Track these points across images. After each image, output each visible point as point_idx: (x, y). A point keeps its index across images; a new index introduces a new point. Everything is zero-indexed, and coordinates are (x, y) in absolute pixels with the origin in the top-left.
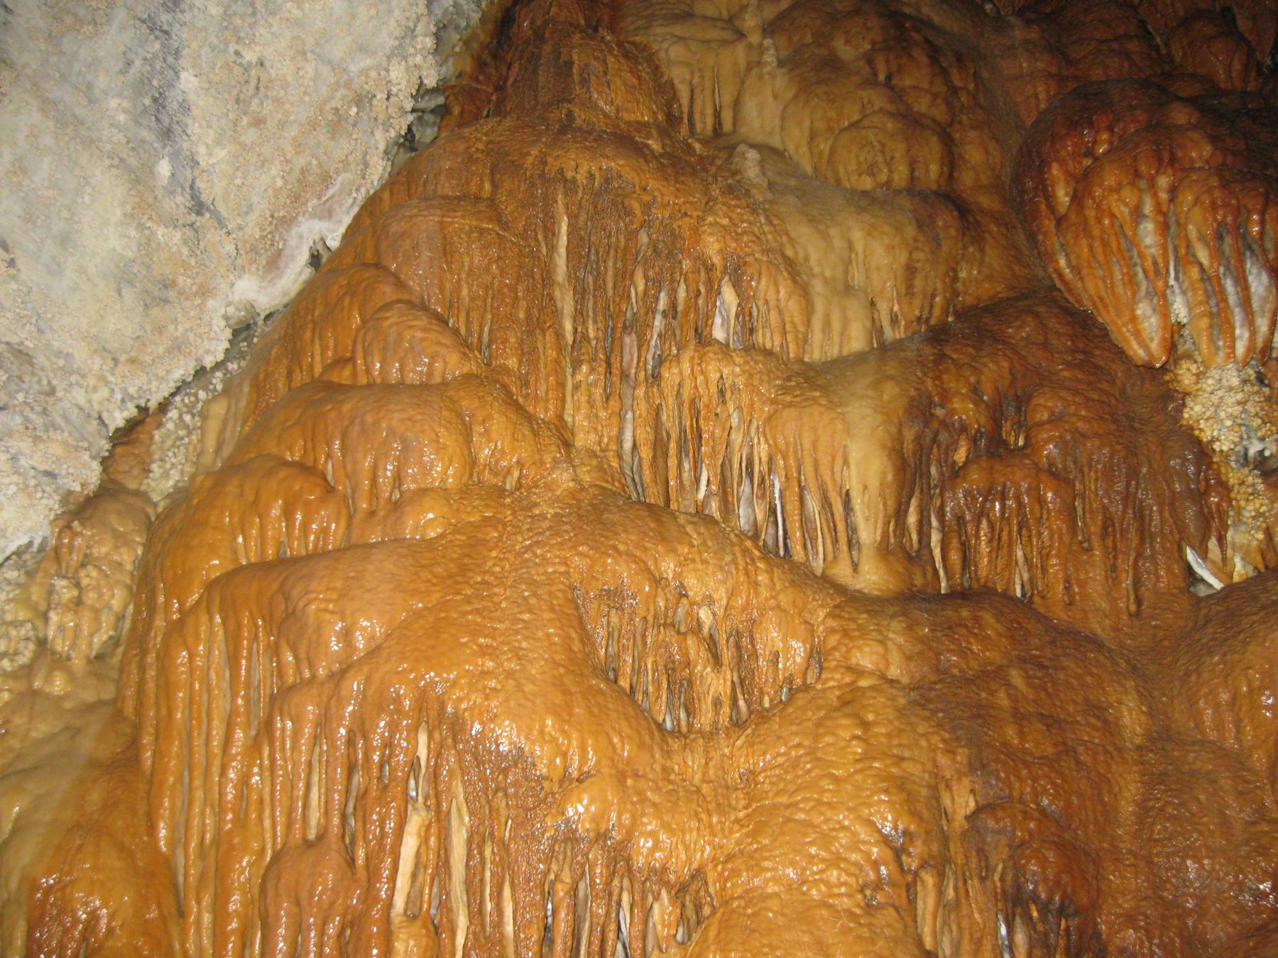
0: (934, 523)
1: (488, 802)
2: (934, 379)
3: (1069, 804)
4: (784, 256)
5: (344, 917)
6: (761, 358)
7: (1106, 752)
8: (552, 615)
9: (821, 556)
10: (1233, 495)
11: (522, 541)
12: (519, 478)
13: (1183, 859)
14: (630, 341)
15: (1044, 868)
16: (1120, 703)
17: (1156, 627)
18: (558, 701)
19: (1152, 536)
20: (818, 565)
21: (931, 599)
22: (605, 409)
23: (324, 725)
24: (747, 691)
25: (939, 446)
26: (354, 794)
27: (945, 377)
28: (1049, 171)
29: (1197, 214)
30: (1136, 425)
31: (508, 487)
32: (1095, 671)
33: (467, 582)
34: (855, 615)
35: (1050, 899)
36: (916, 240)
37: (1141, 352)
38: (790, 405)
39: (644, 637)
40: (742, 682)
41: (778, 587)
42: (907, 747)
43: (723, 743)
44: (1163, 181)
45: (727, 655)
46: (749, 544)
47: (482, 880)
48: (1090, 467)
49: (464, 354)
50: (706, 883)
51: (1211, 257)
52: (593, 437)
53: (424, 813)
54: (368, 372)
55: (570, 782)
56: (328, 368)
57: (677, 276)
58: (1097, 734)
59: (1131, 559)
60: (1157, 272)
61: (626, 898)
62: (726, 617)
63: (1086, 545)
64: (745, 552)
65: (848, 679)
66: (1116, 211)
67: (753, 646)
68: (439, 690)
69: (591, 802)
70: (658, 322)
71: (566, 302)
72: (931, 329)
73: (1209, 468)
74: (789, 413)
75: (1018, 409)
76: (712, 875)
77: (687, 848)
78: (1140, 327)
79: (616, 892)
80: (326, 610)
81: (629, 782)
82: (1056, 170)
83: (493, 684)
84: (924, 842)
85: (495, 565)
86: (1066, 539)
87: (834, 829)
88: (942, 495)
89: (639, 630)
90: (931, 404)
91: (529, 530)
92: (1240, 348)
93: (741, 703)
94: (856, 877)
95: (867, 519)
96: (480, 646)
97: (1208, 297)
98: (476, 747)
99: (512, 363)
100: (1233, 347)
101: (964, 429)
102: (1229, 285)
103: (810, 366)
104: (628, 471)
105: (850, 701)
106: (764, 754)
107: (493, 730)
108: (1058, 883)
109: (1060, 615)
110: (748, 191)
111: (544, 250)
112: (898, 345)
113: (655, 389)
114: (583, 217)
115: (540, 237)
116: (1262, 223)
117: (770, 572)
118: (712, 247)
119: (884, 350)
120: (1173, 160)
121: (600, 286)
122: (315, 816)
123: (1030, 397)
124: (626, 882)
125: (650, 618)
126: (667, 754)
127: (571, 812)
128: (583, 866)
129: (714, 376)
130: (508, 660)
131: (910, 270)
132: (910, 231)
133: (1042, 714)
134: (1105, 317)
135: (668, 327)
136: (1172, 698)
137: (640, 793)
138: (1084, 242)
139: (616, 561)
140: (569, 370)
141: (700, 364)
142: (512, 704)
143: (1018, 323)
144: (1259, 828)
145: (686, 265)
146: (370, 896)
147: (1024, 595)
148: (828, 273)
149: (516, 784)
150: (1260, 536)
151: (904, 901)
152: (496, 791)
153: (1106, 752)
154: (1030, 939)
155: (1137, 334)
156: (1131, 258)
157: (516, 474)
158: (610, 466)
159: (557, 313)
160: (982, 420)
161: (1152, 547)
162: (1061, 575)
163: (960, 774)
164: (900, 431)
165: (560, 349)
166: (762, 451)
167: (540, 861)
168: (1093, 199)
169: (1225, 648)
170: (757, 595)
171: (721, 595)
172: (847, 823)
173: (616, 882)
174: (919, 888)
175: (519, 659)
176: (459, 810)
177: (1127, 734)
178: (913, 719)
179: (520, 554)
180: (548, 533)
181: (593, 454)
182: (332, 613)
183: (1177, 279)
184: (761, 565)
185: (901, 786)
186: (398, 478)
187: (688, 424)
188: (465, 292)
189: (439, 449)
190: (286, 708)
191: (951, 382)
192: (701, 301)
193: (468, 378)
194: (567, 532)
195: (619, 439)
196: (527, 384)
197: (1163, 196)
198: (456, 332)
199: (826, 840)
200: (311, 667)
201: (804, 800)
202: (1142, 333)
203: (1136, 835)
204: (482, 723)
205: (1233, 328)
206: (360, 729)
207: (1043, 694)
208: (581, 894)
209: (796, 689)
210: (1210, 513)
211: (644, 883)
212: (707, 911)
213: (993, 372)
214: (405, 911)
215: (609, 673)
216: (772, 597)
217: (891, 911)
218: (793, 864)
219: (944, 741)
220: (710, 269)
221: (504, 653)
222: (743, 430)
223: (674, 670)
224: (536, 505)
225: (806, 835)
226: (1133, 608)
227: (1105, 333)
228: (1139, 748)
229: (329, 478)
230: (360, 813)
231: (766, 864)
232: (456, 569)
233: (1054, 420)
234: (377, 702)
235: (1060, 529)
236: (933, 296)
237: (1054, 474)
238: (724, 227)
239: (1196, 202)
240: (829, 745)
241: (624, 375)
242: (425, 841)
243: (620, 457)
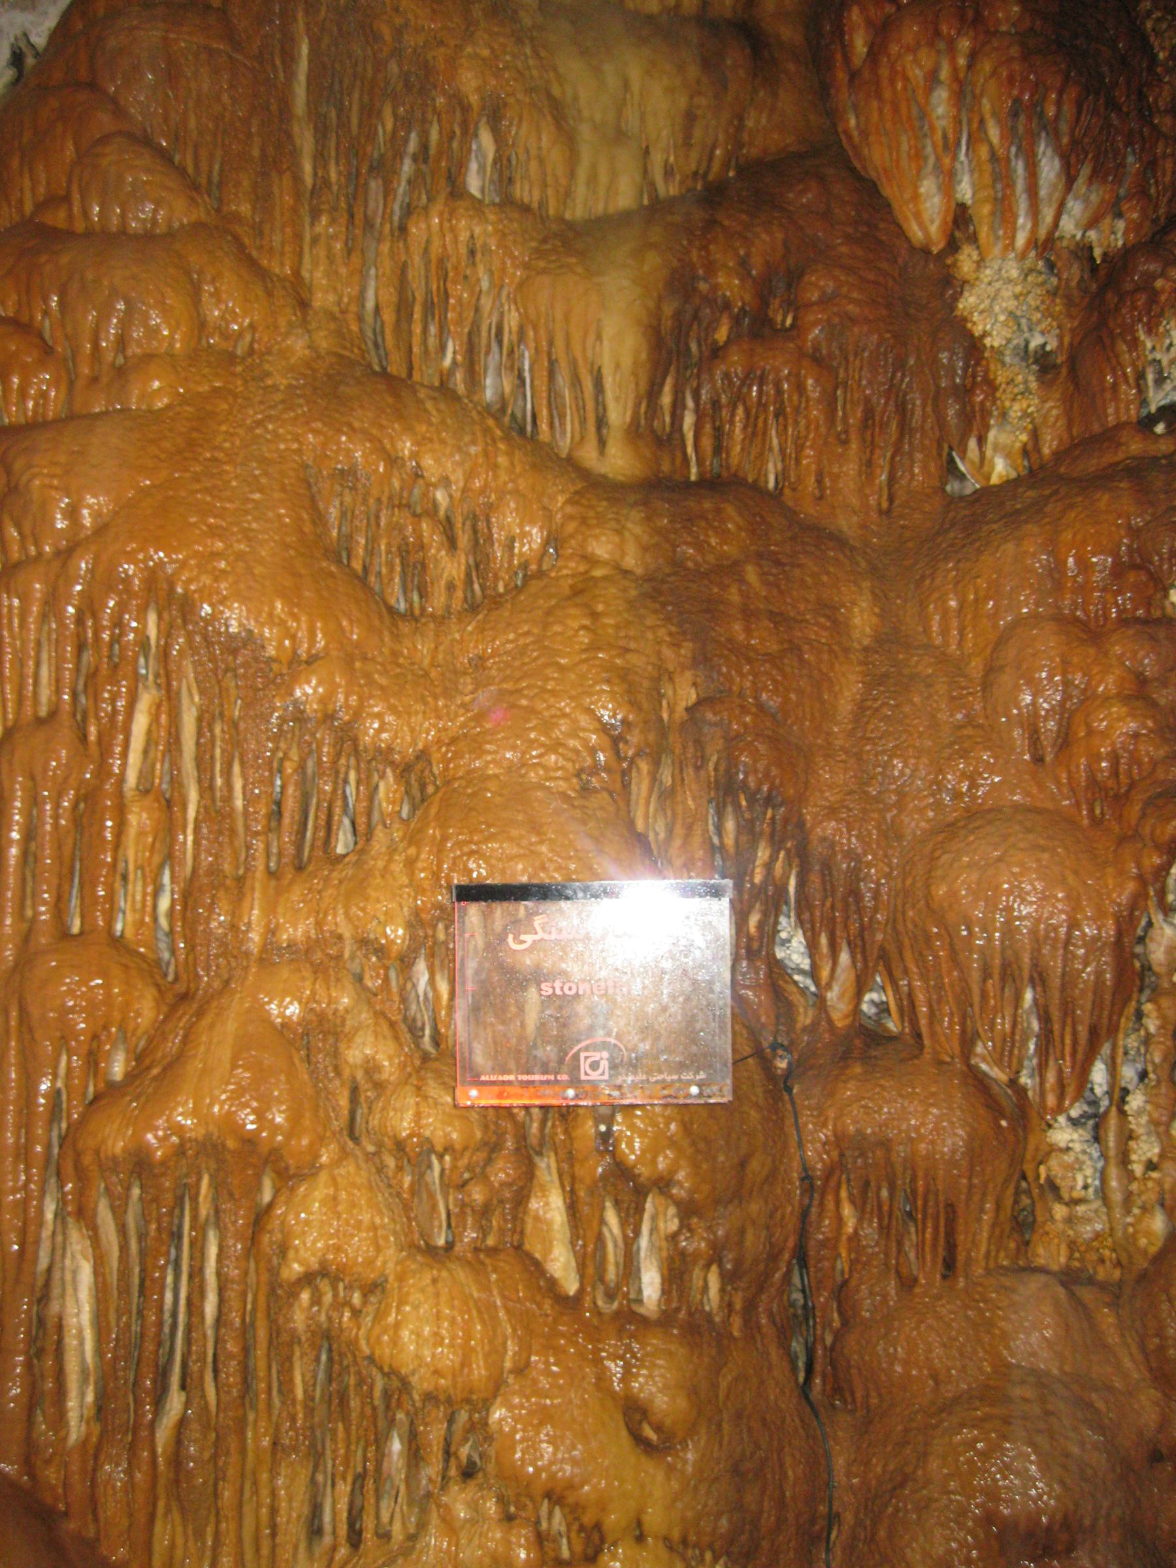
0: (690, 403)
1: (219, 682)
2: (700, 249)
3: (786, 700)
4: (550, 96)
5: (78, 790)
6: (516, 216)
7: (831, 651)
8: (282, 495)
9: (569, 435)
10: (998, 395)
11: (253, 414)
12: (252, 343)
13: (891, 757)
14: (375, 185)
15: (755, 761)
16: (854, 603)
17: (903, 527)
18: (286, 583)
19: (912, 432)
20: (564, 445)
21: (671, 490)
22: (347, 265)
23: (53, 603)
24: (482, 576)
25: (699, 325)
26: (84, 671)
27: (712, 247)
28: (849, 11)
29: (992, 85)
30: (912, 311)
31: (239, 352)
32: (832, 569)
33: (195, 459)
34: (594, 502)
35: (759, 790)
36: (698, 82)
37: (920, 234)
38: (544, 271)
39: (378, 517)
40: (477, 566)
41: (518, 470)
42: (635, 639)
43: (454, 628)
44: (965, 44)
45: (464, 540)
46: (491, 422)
47: (212, 757)
48: (856, 355)
49: (192, 199)
50: (430, 764)
51: (1002, 137)
52: (331, 298)
53: (154, 691)
54: (86, 214)
55: (299, 665)
56: (39, 207)
57: (429, 116)
58: (825, 634)
59: (889, 455)
60: (946, 146)
61: (352, 776)
62: (462, 500)
63: (843, 436)
64: (486, 431)
65: (582, 568)
66: (910, 74)
67: (489, 529)
68: (169, 569)
69: (319, 684)
70: (407, 167)
71: (305, 140)
72: (708, 187)
73: (977, 364)
74: (546, 280)
75: (789, 286)
76: (436, 756)
77: (412, 730)
78: (922, 207)
79: (343, 770)
80: (51, 487)
81: (358, 665)
82: (855, 14)
83: (223, 565)
84: (642, 732)
85: (225, 440)
86: (823, 430)
87: (553, 716)
88: (698, 376)
89: (373, 510)
90: (695, 278)
91: (261, 402)
92: (1021, 240)
93: (476, 587)
94: (573, 762)
95: (617, 399)
96: (210, 526)
97: (995, 181)
98: (206, 628)
99: (245, 209)
100: (1013, 238)
101: (727, 306)
102: (1020, 167)
103: (570, 225)
104: (370, 334)
105: (582, 590)
106: (493, 640)
107: (222, 612)
108: (767, 775)
109: (809, 510)
110: (516, 12)
111: (281, 76)
112: (672, 202)
113: (401, 245)
114: (326, 40)
115: (278, 62)
116: (1059, 103)
117: (510, 454)
118: (469, 82)
119: (655, 209)
120: (978, 20)
121: (344, 124)
122: (45, 694)
123: (802, 275)
124: (353, 761)
125: (385, 499)
126: (397, 637)
127: (298, 693)
128: (310, 744)
129: (464, 236)
130: (238, 541)
131: (690, 118)
132: (693, 71)
133: (771, 612)
134: (888, 191)
135: (418, 174)
136: (906, 601)
137: (368, 676)
138: (875, 104)
139: (350, 440)
140: (307, 220)
141: (450, 221)
142: (242, 586)
143: (801, 187)
144: (965, 732)
145: (441, 101)
146: (103, 771)
147: (776, 487)
148: (598, 117)
149: (245, 665)
150: (1024, 437)
151: (618, 786)
152: (226, 671)
153: (831, 651)
154: (738, 825)
155: (918, 215)
156: (922, 128)
157: (248, 338)
158: (350, 331)
159: (295, 154)
160: (747, 297)
161: (910, 443)
162: (814, 467)
163: (683, 668)
164: (659, 308)
165: (297, 195)
166: (512, 320)
167: (268, 739)
168: (889, 56)
169: (960, 556)
170: (496, 477)
171: (458, 477)
172: (568, 710)
173: (343, 761)
174: (634, 774)
175: (249, 540)
176: (189, 689)
177: (856, 635)
178: (642, 611)
179: (251, 429)
180: (280, 407)
181: (332, 317)
182: (57, 488)
183: (967, 154)
184: (502, 446)
185: (624, 678)
186: (122, 342)
187: (435, 287)
188: (192, 123)
189: (166, 312)
190: (12, 585)
191: (717, 252)
192: (455, 145)
193: (198, 226)
194: (301, 406)
195: (361, 298)
196: (261, 234)
197: (962, 61)
198: (182, 171)
199: (547, 726)
200: (37, 544)
201: (527, 687)
202: (925, 214)
203: (851, 734)
204: (211, 605)
205: (1015, 217)
206: (89, 608)
207: (775, 592)
208: (310, 771)
209: (531, 575)
210: (973, 412)
211: (369, 762)
212: (430, 789)
213: (766, 243)
214: (138, 785)
215: (339, 553)
216: (512, 481)
217: (605, 795)
218: (514, 748)
219: (670, 634)
220: (466, 108)
221: (233, 534)
222: (495, 290)
223: (408, 552)
224: (268, 374)
225: (528, 720)
226: (885, 505)
228: (866, 649)
229: (47, 336)
230: (90, 690)
231: (488, 747)
232: (185, 439)
233: (825, 301)
234: (105, 580)
235: (817, 420)
236: (714, 148)
237: (818, 360)
238: (483, 59)
239: (994, 73)
240: (557, 634)
241: (369, 224)
242: (155, 719)
243: (360, 319)
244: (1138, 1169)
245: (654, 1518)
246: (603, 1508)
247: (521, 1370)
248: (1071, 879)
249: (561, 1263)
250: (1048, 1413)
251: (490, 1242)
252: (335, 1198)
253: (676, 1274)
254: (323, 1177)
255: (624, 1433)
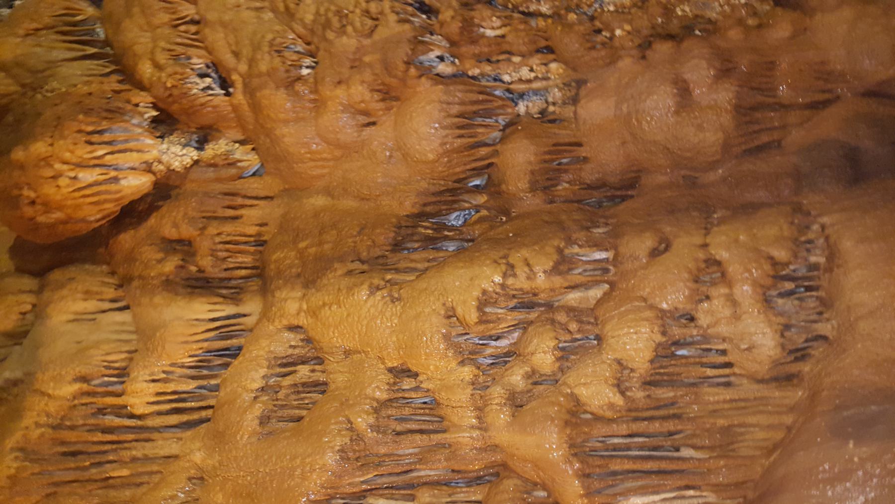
38: (164, 348)
81: (351, 402)
105: (313, 313)
134: (126, 202)
227: (132, 203)
244: (533, 75)
245: (698, 240)
246: (696, 260)
247: (645, 300)
248: (423, 104)
249: (596, 293)
250: (632, 97)
251: (592, 320)
252: (585, 384)
253: (598, 245)
254: (576, 391)
255: (664, 256)
